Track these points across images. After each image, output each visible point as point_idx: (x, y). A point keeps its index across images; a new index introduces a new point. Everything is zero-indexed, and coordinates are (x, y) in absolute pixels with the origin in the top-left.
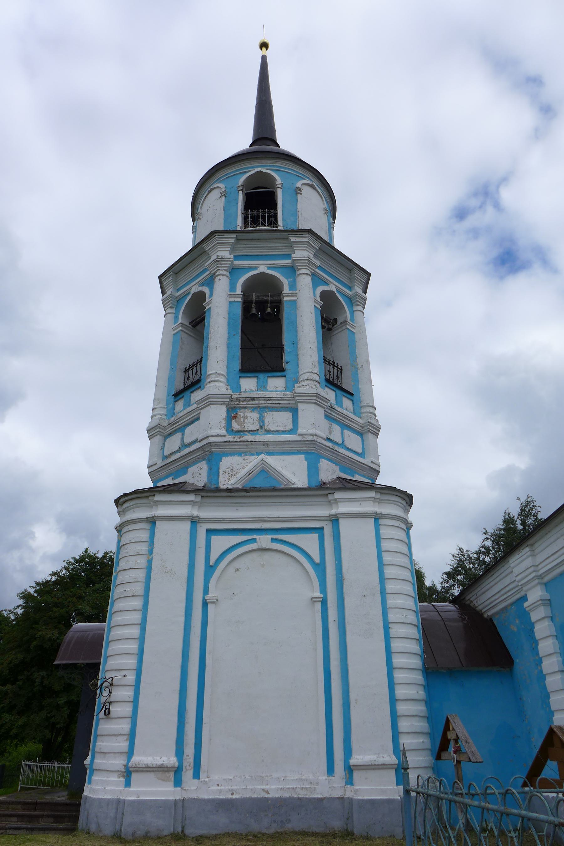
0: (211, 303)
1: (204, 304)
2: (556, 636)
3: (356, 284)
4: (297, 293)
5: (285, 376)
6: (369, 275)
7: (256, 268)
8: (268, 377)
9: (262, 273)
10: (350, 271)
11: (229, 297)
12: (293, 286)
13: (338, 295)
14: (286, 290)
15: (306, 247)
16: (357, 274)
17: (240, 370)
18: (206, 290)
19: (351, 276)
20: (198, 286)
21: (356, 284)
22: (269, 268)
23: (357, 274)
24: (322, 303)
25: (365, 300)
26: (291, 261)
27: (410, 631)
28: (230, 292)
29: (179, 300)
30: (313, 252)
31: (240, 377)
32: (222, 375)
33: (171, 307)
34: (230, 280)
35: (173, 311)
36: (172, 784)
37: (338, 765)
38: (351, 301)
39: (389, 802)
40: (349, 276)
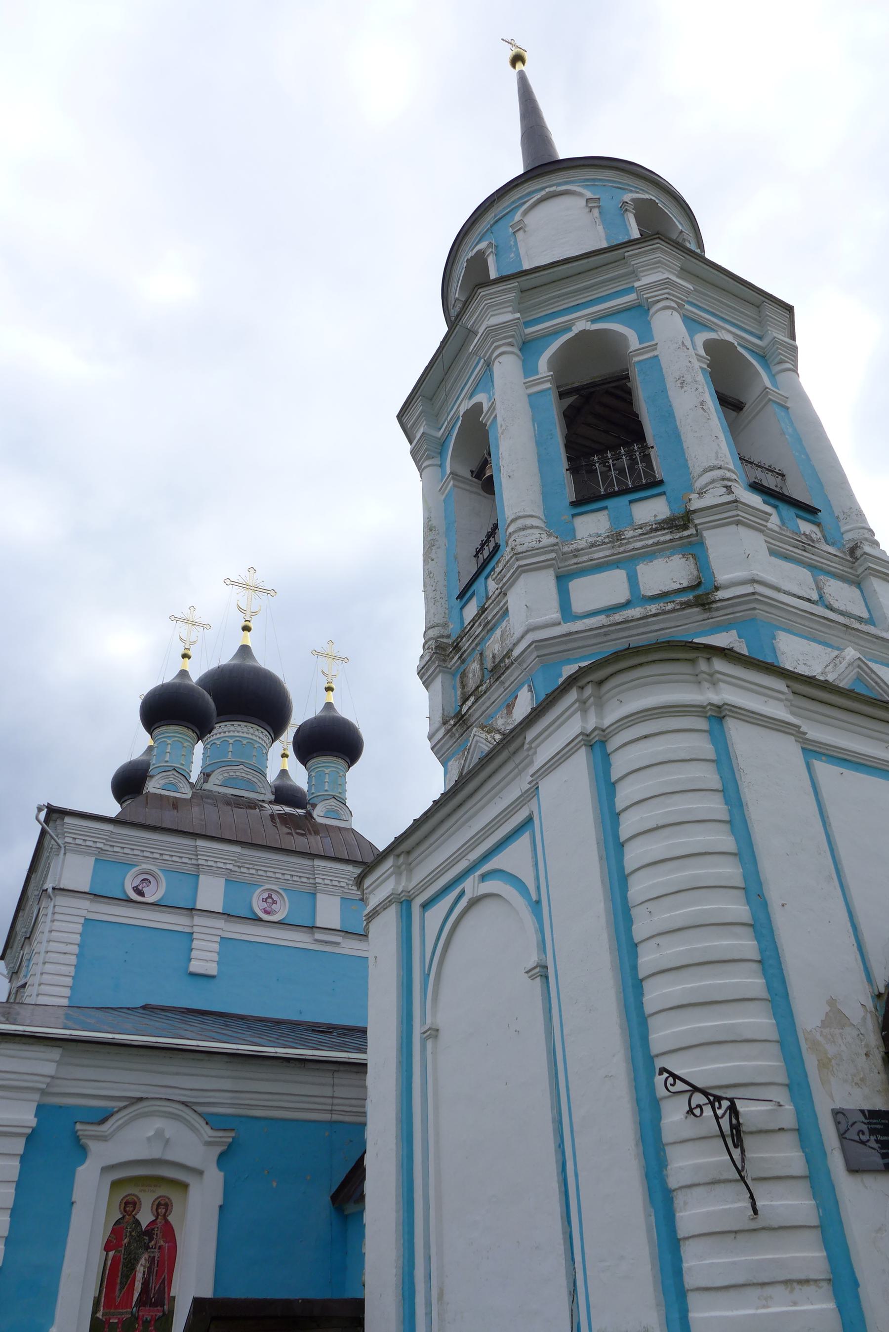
0: (494, 409)
1: (481, 419)
2: (787, 1085)
3: (769, 328)
4: (657, 344)
5: (664, 493)
6: (790, 309)
7: (567, 328)
8: (631, 502)
9: (583, 332)
10: (758, 307)
11: (527, 388)
12: (645, 333)
13: (739, 349)
14: (634, 343)
15: (668, 293)
16: (769, 310)
17: (571, 503)
18: (480, 397)
19: (760, 317)
20: (467, 401)
21: (769, 328)
22: (594, 321)
23: (769, 310)
24: (709, 358)
25: (795, 348)
26: (635, 294)
28: (525, 378)
29: (443, 444)
30: (676, 265)
31: (574, 516)
32: (539, 518)
33: (429, 457)
34: (523, 361)
35: (437, 461)
36: (207, 1292)
37: (629, 1150)
38: (766, 360)
39: (615, 809)
40: (756, 317)
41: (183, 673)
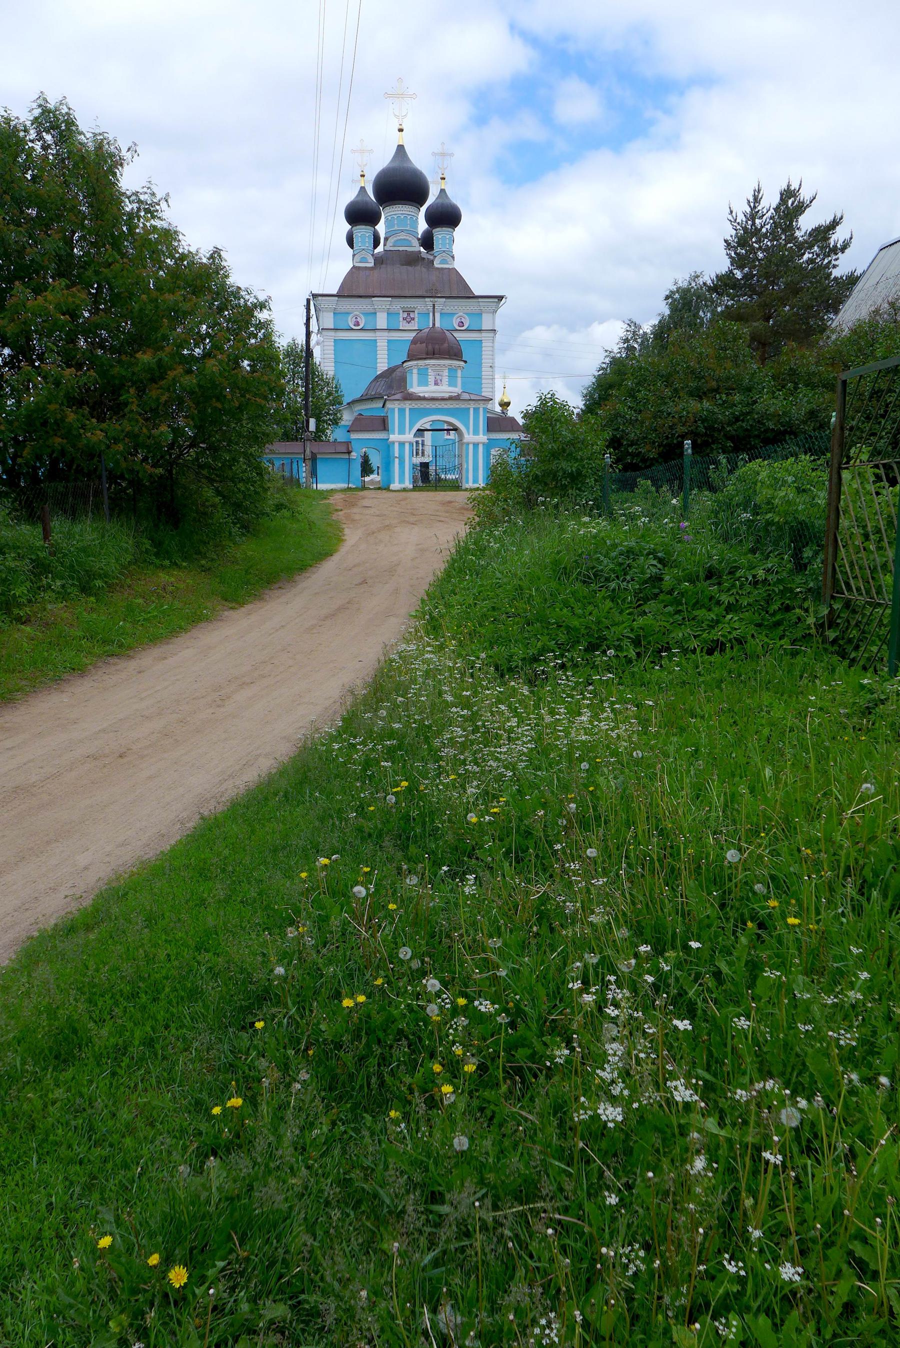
27: (741, 1094)
41: (363, 189)
